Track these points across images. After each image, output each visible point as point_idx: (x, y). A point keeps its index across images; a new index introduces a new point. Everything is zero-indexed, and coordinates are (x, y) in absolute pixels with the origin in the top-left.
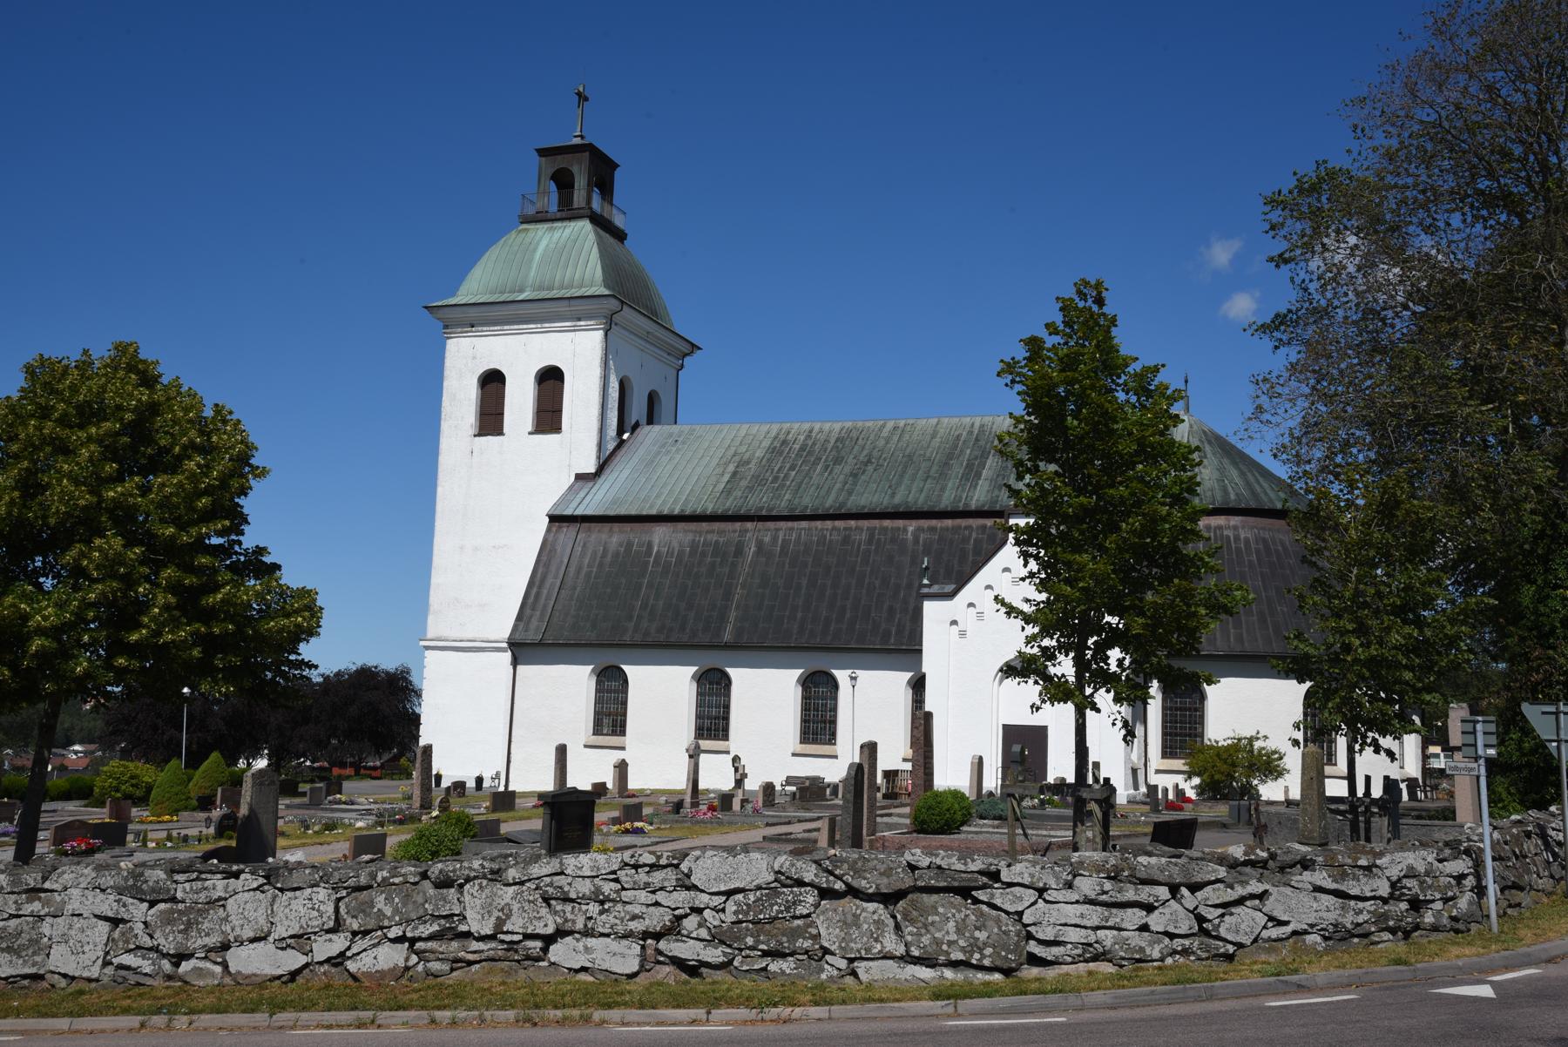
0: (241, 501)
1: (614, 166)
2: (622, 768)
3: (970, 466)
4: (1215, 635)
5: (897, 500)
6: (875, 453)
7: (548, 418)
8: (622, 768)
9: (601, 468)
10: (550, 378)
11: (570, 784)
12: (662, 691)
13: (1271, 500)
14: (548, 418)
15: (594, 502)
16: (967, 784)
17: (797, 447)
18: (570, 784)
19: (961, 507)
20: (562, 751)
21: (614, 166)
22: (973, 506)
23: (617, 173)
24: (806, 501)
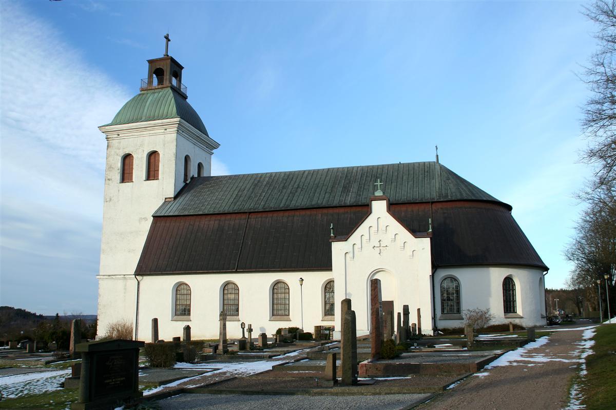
0: (102, 332)
1: (182, 68)
2: (187, 329)
3: (344, 187)
4: (227, 320)
5: (313, 203)
6: (301, 184)
7: (152, 173)
8: (187, 329)
9: (176, 197)
10: (153, 157)
11: (160, 338)
12: (205, 288)
13: (481, 197)
14: (152, 173)
15: (173, 210)
16: (313, 332)
17: (265, 183)
18: (160, 338)
19: (343, 204)
20: (155, 321)
21: (182, 68)
22: (348, 204)
23: (183, 71)
24: (272, 205)
